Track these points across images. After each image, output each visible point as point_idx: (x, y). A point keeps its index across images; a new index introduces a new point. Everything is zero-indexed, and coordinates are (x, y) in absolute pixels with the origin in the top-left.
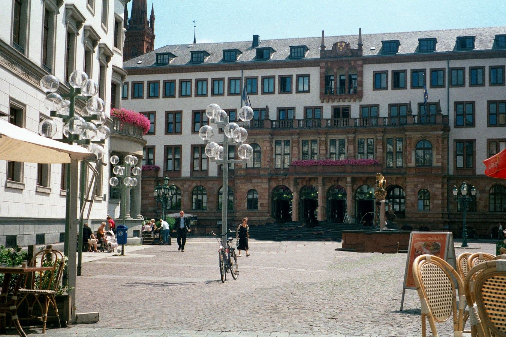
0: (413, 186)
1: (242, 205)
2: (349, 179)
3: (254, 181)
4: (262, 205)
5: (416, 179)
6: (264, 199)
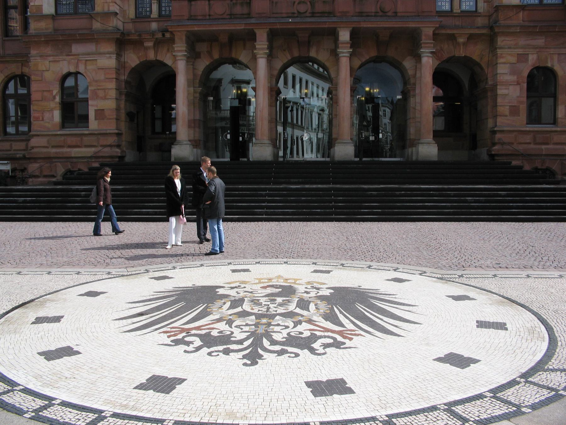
0: (513, 60)
1: (47, 115)
2: (344, 36)
3: (77, 48)
4: (100, 114)
5: (522, 41)
6: (105, 98)
